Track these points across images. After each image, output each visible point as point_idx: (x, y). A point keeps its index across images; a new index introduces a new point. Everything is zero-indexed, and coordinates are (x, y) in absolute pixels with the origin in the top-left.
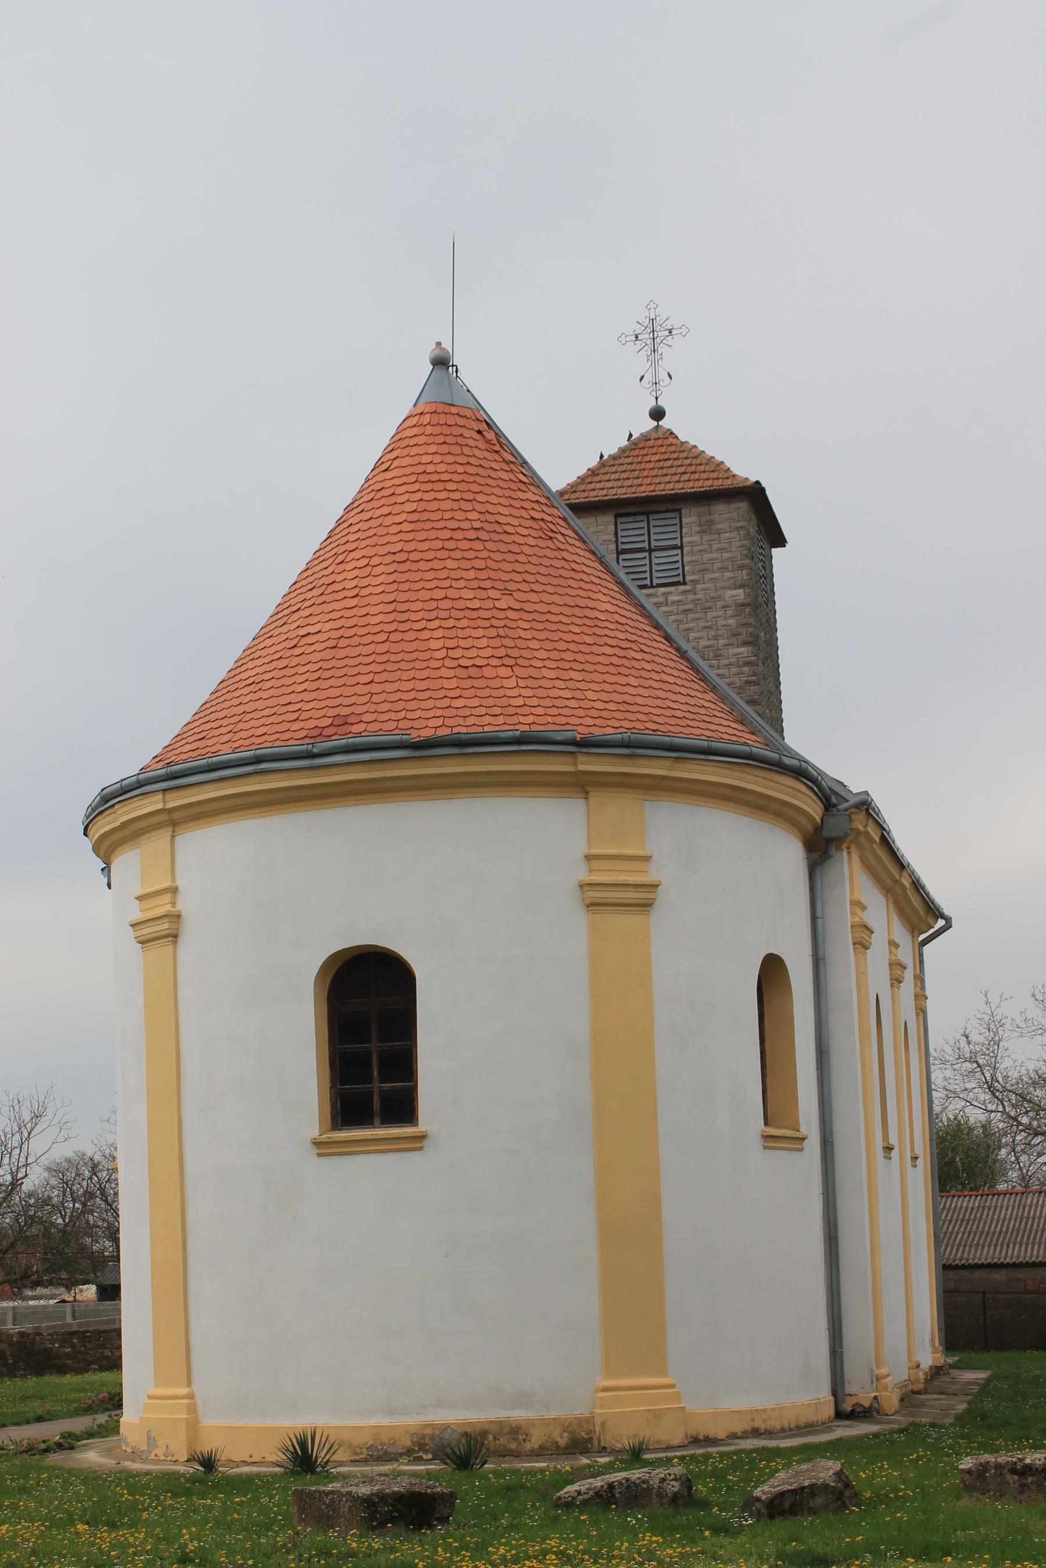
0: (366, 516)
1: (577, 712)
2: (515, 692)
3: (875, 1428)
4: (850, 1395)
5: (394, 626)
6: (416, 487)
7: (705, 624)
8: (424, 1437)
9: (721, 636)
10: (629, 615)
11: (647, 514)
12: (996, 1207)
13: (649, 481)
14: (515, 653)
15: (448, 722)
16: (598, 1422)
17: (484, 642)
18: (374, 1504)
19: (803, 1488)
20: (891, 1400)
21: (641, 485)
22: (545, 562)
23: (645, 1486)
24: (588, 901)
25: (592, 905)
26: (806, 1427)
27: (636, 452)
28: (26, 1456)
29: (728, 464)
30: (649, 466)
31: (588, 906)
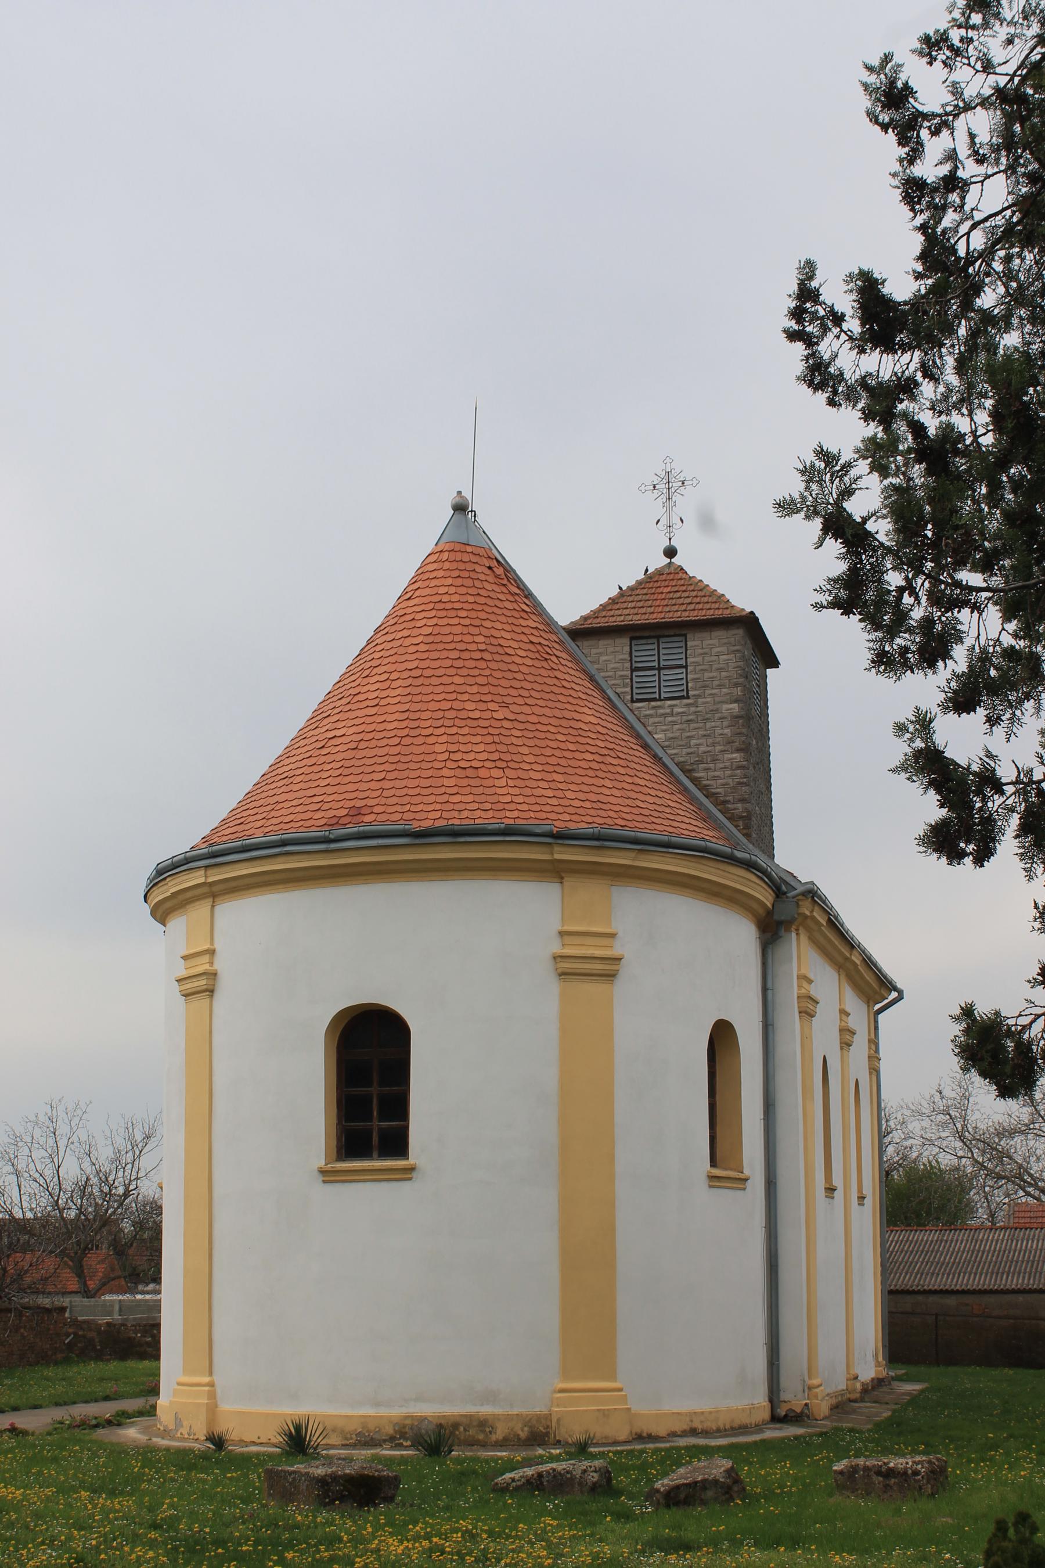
0: (389, 637)
1: (556, 809)
2: (505, 791)
3: (800, 1431)
4: (785, 1402)
5: (405, 732)
6: (433, 613)
7: (705, 733)
8: (404, 1426)
9: (718, 743)
10: (610, 726)
11: (658, 637)
12: (952, 1241)
13: (660, 609)
14: (507, 757)
15: (445, 815)
16: (554, 1420)
17: (481, 747)
18: (328, 1484)
19: (696, 1483)
20: (822, 1408)
21: (653, 613)
22: (539, 679)
23: (569, 1476)
24: (560, 971)
25: (563, 975)
26: (740, 1428)
27: (651, 585)
28: (77, 1430)
29: (728, 596)
30: (660, 597)
31: (560, 975)
